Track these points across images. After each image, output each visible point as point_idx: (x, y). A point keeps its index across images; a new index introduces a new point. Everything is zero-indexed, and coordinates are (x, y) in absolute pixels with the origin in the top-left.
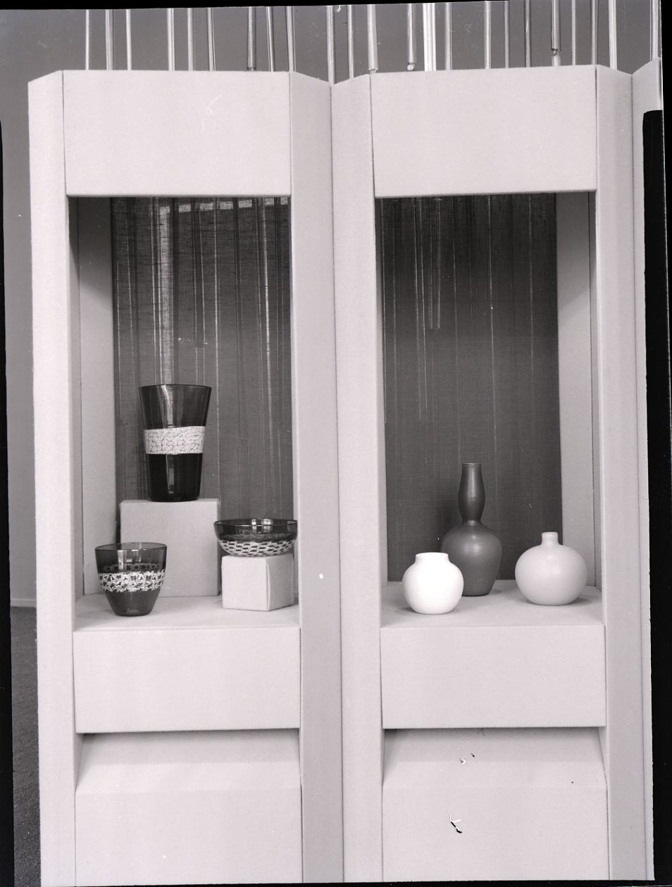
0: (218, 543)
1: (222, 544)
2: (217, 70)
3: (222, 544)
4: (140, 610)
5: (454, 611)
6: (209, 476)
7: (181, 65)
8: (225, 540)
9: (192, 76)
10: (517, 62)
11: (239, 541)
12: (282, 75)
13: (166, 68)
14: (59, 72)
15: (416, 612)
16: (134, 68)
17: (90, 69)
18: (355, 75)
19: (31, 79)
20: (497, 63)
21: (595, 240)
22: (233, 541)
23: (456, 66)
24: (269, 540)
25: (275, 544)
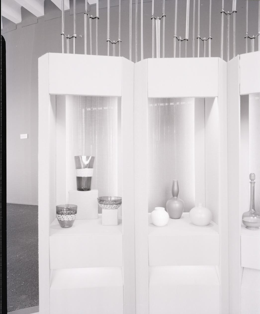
0: (99, 206)
1: (99, 205)
2: (116, 56)
3: (99, 205)
4: (69, 226)
5: (166, 225)
6: (93, 183)
7: (65, 52)
8: (100, 203)
9: (68, 55)
10: (183, 56)
11: (105, 204)
12: (216, 59)
13: (62, 52)
14: (48, 53)
15: (157, 226)
16: (76, 53)
17: (211, 57)
18: (144, 58)
19: (40, 55)
20: (177, 56)
21: (65, 104)
22: (102, 204)
23: (166, 57)
24: (114, 204)
25: (116, 206)
